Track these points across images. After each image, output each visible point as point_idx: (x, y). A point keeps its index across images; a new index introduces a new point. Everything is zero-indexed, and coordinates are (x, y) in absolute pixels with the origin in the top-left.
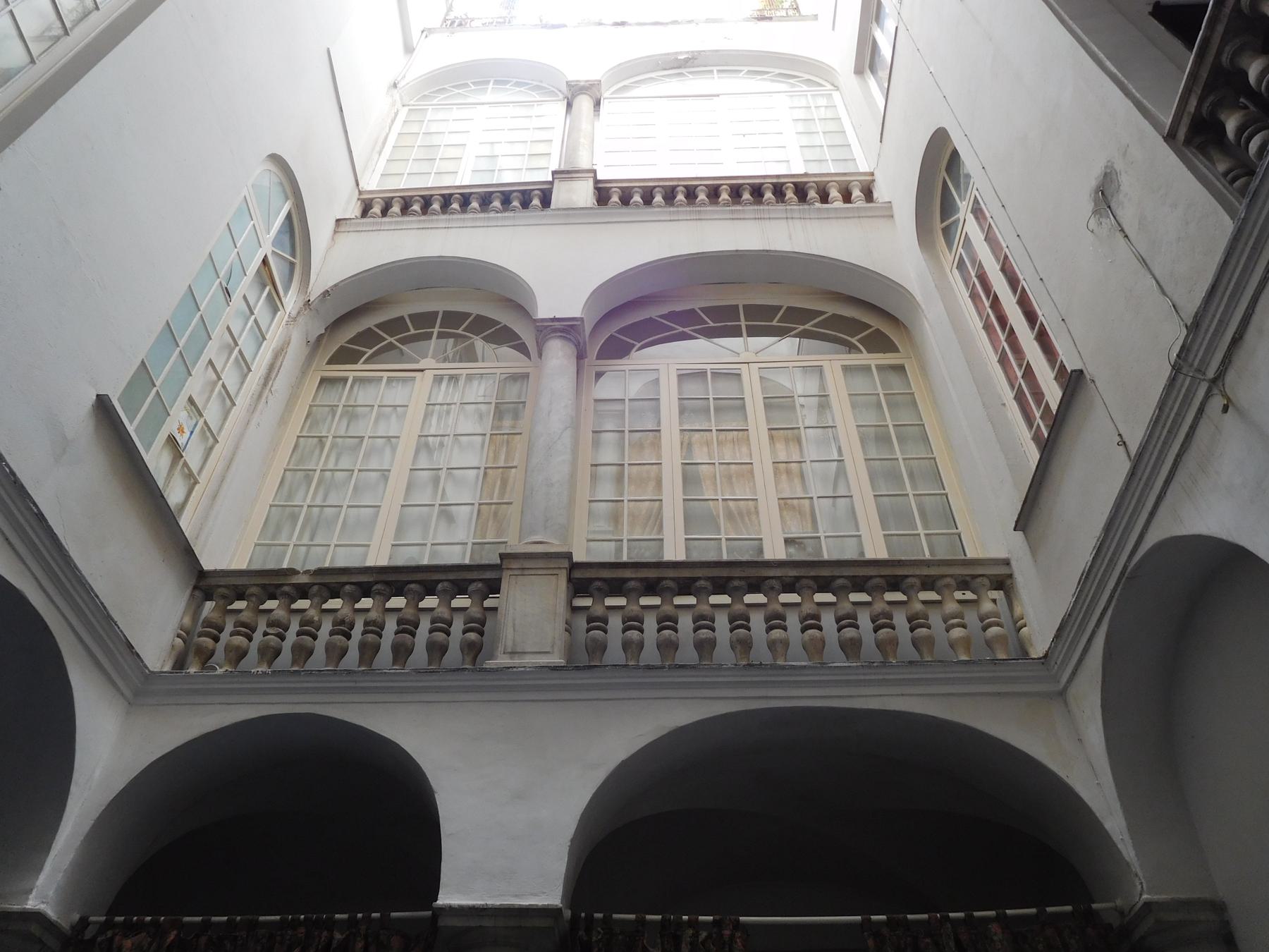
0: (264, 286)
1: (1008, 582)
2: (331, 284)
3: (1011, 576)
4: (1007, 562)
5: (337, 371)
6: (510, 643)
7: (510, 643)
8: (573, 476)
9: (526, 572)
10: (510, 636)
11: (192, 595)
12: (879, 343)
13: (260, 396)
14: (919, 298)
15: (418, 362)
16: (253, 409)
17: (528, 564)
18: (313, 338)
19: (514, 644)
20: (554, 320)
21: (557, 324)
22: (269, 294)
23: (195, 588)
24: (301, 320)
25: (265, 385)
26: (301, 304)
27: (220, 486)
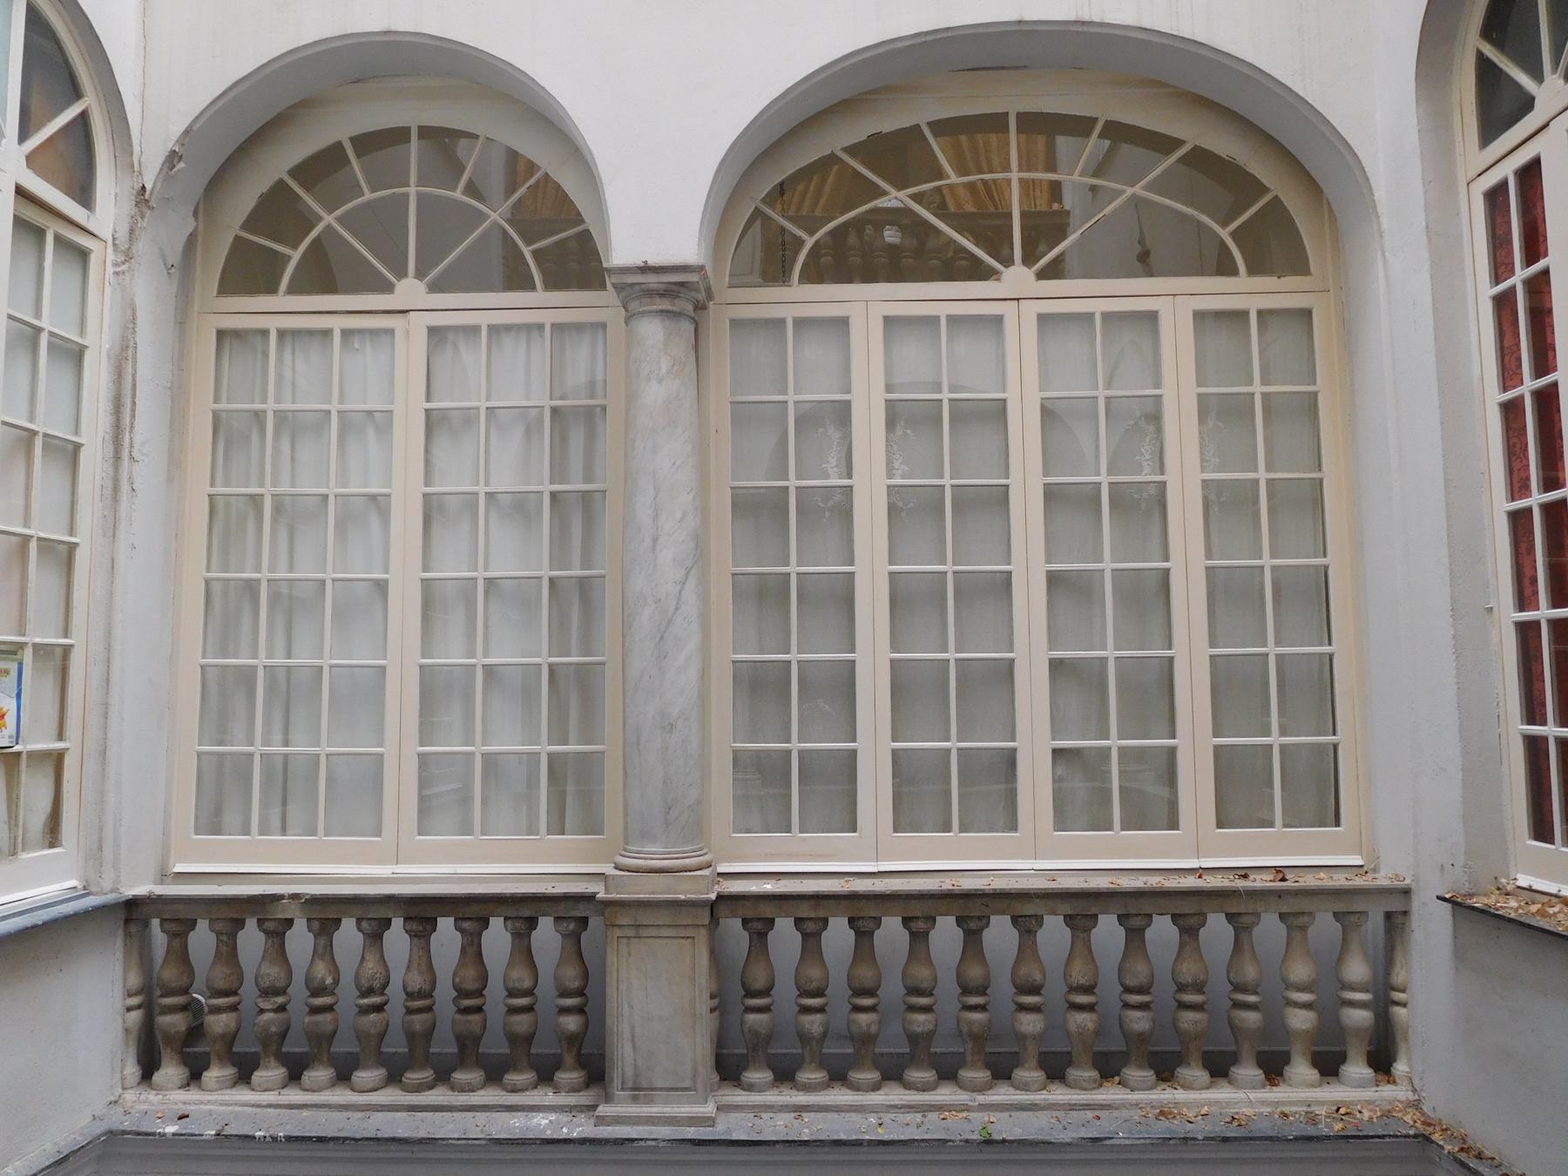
0: (40, 233)
1: (1400, 920)
2: (177, 129)
3: (1405, 913)
4: (1406, 892)
5: (249, 311)
6: (629, 1072)
7: (629, 1072)
8: (703, 697)
9: (644, 932)
10: (629, 1060)
11: (127, 934)
12: (1272, 245)
13: (116, 489)
14: (1380, 194)
15: (388, 288)
16: (111, 527)
17: (646, 918)
18: (175, 256)
19: (637, 1075)
20: (646, 269)
21: (651, 280)
22: (58, 239)
23: (127, 921)
24: (142, 247)
25: (117, 457)
26: (128, 206)
27: (105, 728)
